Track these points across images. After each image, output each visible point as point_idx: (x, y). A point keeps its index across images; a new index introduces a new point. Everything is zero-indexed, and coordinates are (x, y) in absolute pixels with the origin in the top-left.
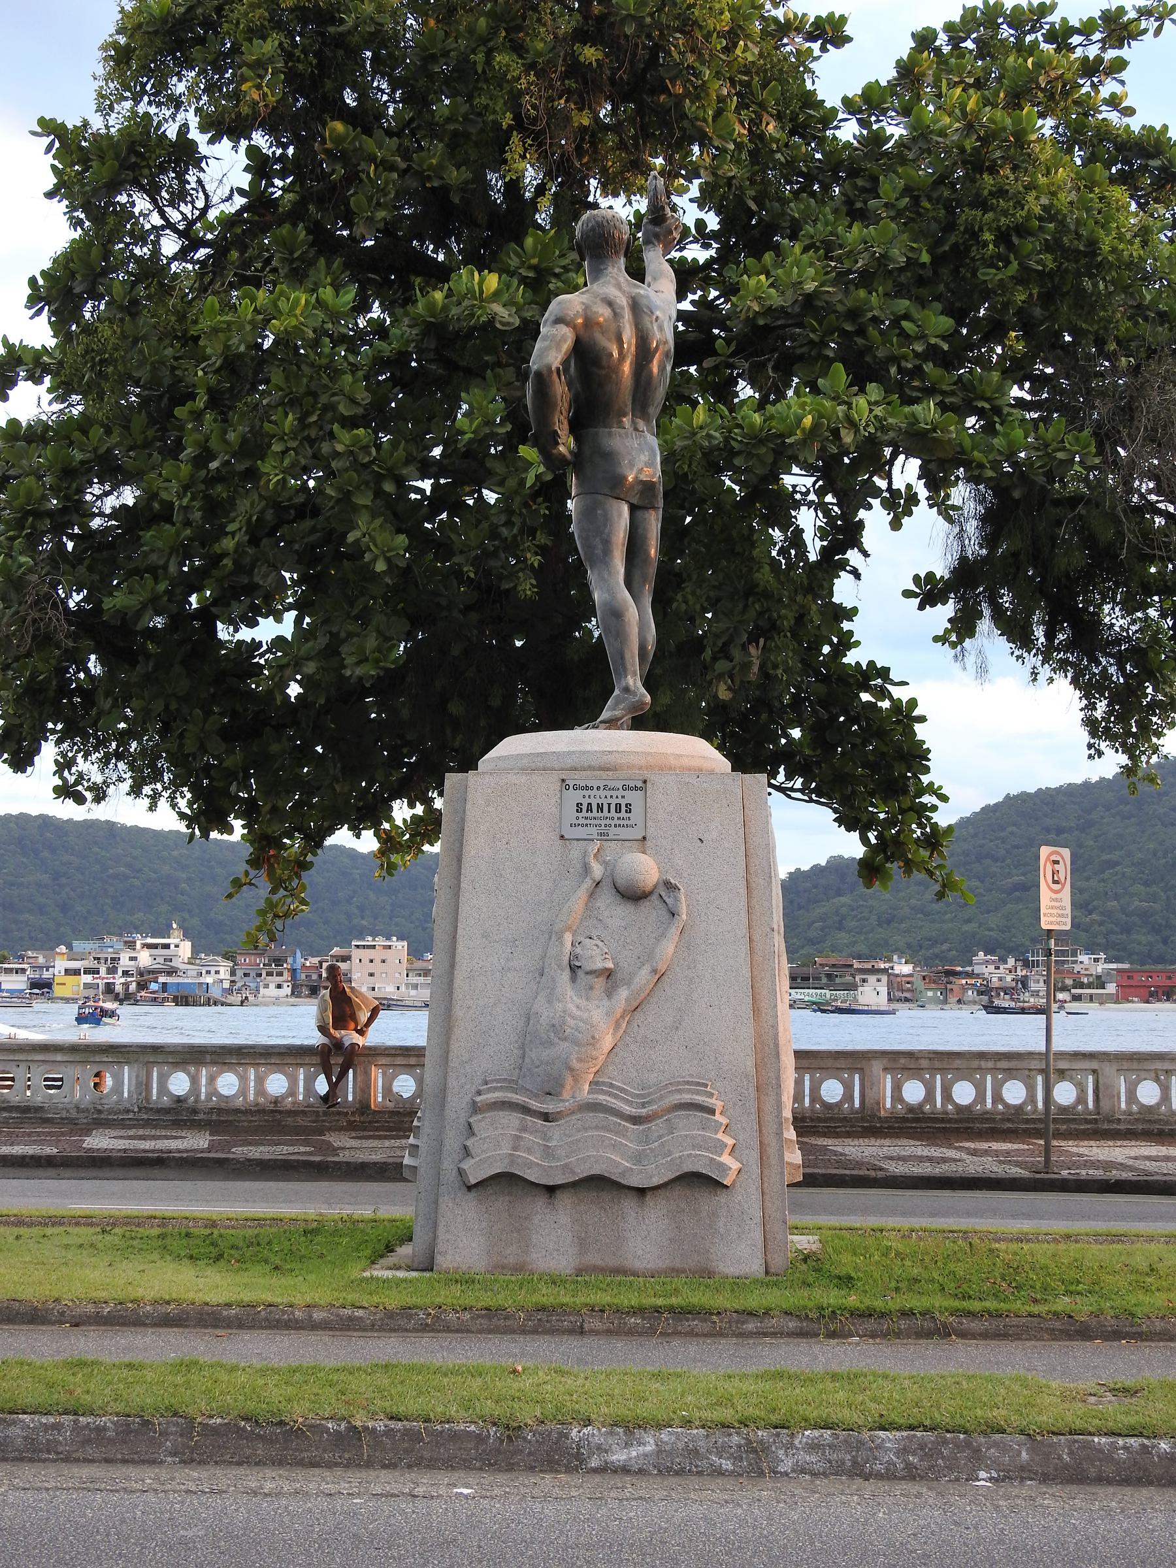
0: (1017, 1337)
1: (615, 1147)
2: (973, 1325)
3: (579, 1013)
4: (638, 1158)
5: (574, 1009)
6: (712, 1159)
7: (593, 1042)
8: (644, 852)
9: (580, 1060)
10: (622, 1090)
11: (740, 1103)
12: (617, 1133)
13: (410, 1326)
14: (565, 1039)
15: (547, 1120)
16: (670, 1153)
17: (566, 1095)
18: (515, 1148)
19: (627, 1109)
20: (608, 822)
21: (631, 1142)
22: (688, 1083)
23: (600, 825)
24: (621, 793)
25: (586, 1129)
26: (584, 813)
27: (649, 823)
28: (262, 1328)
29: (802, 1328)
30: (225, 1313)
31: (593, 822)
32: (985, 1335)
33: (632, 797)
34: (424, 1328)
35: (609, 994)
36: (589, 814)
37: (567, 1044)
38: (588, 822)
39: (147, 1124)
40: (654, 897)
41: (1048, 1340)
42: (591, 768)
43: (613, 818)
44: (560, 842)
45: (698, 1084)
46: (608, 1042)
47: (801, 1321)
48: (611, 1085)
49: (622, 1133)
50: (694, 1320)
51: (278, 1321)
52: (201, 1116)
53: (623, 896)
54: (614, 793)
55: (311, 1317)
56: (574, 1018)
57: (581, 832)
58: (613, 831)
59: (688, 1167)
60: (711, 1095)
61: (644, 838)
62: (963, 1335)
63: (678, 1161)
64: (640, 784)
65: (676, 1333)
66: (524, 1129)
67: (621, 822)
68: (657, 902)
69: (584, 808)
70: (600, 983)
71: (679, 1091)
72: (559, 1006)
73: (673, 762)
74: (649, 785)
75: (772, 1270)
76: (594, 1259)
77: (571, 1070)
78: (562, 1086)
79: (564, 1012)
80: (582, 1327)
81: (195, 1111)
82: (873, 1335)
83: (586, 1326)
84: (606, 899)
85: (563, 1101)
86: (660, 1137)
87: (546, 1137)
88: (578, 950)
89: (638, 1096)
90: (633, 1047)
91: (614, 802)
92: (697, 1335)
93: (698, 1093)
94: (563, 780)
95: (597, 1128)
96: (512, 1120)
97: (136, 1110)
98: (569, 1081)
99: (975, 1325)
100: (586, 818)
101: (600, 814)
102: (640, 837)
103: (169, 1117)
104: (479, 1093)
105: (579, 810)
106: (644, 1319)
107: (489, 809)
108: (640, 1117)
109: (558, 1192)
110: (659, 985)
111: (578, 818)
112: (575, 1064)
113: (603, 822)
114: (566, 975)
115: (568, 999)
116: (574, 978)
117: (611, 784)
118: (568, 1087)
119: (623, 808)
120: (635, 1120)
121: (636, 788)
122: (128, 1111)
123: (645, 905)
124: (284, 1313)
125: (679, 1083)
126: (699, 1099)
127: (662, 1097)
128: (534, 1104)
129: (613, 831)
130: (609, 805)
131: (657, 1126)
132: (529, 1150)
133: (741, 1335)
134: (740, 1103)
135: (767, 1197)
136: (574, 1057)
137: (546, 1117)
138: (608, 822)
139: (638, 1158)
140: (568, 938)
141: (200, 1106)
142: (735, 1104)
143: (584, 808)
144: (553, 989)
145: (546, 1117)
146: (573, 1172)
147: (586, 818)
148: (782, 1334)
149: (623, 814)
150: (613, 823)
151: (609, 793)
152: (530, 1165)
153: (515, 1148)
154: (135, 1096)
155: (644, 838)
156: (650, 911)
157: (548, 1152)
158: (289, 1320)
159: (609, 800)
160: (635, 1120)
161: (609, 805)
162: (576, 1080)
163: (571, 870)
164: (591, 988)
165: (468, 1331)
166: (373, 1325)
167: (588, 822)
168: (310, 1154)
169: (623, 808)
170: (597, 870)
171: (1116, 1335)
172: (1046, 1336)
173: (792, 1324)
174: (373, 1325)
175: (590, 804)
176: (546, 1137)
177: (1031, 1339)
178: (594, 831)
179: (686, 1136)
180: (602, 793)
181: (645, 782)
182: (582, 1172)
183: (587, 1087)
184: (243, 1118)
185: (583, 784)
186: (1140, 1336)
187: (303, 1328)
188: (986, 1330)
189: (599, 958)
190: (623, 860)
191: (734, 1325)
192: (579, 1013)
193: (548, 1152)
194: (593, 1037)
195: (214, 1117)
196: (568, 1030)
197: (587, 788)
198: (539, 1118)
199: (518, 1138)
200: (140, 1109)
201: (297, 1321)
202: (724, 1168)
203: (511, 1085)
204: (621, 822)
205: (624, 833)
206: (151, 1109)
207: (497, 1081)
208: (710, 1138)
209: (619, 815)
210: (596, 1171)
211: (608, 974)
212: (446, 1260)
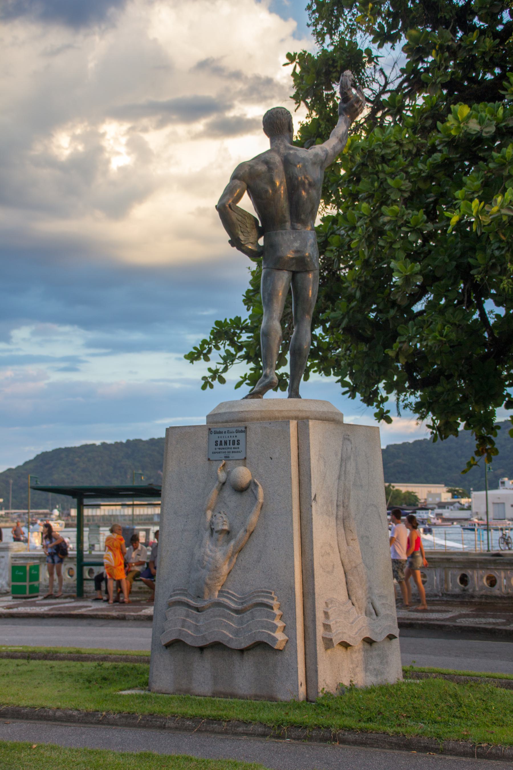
0: (372, 746)
1: (227, 626)
2: (350, 736)
3: (211, 554)
4: (236, 633)
5: (209, 552)
6: (269, 634)
7: (217, 569)
8: (245, 466)
9: (210, 579)
10: (233, 595)
11: (288, 603)
12: (228, 619)
13: (93, 721)
14: (204, 568)
15: (198, 611)
16: (251, 630)
17: (207, 598)
18: (183, 626)
19: (233, 605)
20: (229, 450)
21: (234, 623)
22: (263, 592)
23: (225, 452)
24: (235, 434)
25: (215, 616)
26: (219, 446)
27: (248, 450)
28: (35, 719)
29: (265, 732)
30: (23, 711)
31: (223, 450)
32: (355, 743)
33: (240, 436)
34: (99, 722)
35: (228, 541)
36: (221, 447)
37: (205, 570)
38: (220, 451)
39: (447, 603)
40: (249, 490)
41: (388, 749)
42: (233, 421)
43: (231, 448)
44: (208, 462)
45: (267, 592)
46: (225, 569)
47: (265, 728)
48: (228, 593)
49: (230, 618)
50: (215, 724)
51: (42, 716)
52: (476, 600)
53: (236, 490)
54: (232, 435)
55: (55, 714)
56: (208, 556)
57: (217, 456)
58: (231, 455)
59: (258, 639)
60: (273, 599)
61: (245, 458)
62: (343, 742)
63: (254, 635)
64: (243, 429)
65: (206, 731)
66: (187, 616)
67: (235, 450)
68: (250, 493)
69: (219, 443)
70: (222, 537)
71: (259, 596)
72: (202, 550)
73: (277, 414)
74: (248, 429)
75: (310, 699)
76: (221, 688)
77: (207, 584)
78: (203, 593)
79: (204, 553)
80: (165, 725)
81: (472, 597)
82: (298, 738)
83: (167, 725)
84: (227, 492)
85: (205, 601)
86: (248, 621)
87: (197, 621)
88: (214, 520)
89: (240, 599)
90: (239, 572)
91: (232, 439)
92: (216, 733)
93: (267, 597)
94: (210, 429)
95: (219, 616)
96: (182, 611)
97: (440, 595)
98: (206, 590)
99: (351, 737)
100: (219, 449)
101: (226, 446)
102: (243, 458)
103: (458, 600)
104: (171, 596)
105: (216, 445)
106: (193, 722)
107: (178, 446)
108: (239, 610)
109: (205, 650)
110: (251, 538)
111: (216, 449)
112: (209, 582)
113: (227, 451)
114: (207, 534)
115: (207, 546)
116: (212, 535)
117: (231, 430)
118: (207, 594)
119: (236, 442)
120: (237, 612)
121: (242, 431)
122: (436, 596)
123: (245, 494)
124: (45, 711)
125: (259, 592)
126: (265, 600)
127: (250, 599)
128: (192, 602)
129: (231, 455)
130: (230, 441)
131: (247, 615)
132: (189, 628)
133: (236, 734)
134: (288, 603)
135: (308, 656)
136: (207, 577)
137: (198, 609)
138: (229, 450)
139: (236, 633)
140: (209, 513)
141: (476, 594)
142: (285, 604)
143: (219, 443)
144: (202, 541)
145: (198, 609)
146: (206, 640)
147: (219, 449)
148: (255, 734)
149: (236, 446)
150: (231, 450)
151: (229, 435)
152: (188, 635)
153: (183, 626)
154: (439, 587)
155: (245, 458)
156: (246, 497)
157: (197, 629)
158: (46, 716)
159: (230, 439)
160: (237, 612)
161: (230, 441)
162: (210, 590)
163: (213, 477)
164: (218, 540)
165: (117, 725)
166: (79, 720)
167: (220, 451)
168: (504, 624)
169: (236, 442)
170: (222, 476)
171: (426, 749)
172: (387, 746)
173: (261, 730)
174: (79, 720)
175: (221, 441)
176: (197, 621)
177: (378, 747)
178: (223, 455)
179: (259, 621)
180: (227, 435)
181: (246, 428)
182: (210, 640)
183: (217, 593)
184: (500, 601)
185: (218, 430)
186: (443, 752)
187: (50, 720)
188: (356, 739)
189: (220, 524)
190: (234, 471)
191: (233, 728)
192: (211, 554)
193: (197, 629)
194: (216, 567)
195: (483, 600)
196: (205, 563)
197: (220, 432)
198: (195, 610)
199: (184, 621)
200: (443, 594)
201: (49, 716)
202: (275, 639)
203: (184, 592)
204: (235, 450)
205: (236, 456)
206: (449, 595)
207: (178, 590)
208: (270, 622)
209: (234, 446)
210: (216, 640)
211: (228, 532)
212: (156, 686)
